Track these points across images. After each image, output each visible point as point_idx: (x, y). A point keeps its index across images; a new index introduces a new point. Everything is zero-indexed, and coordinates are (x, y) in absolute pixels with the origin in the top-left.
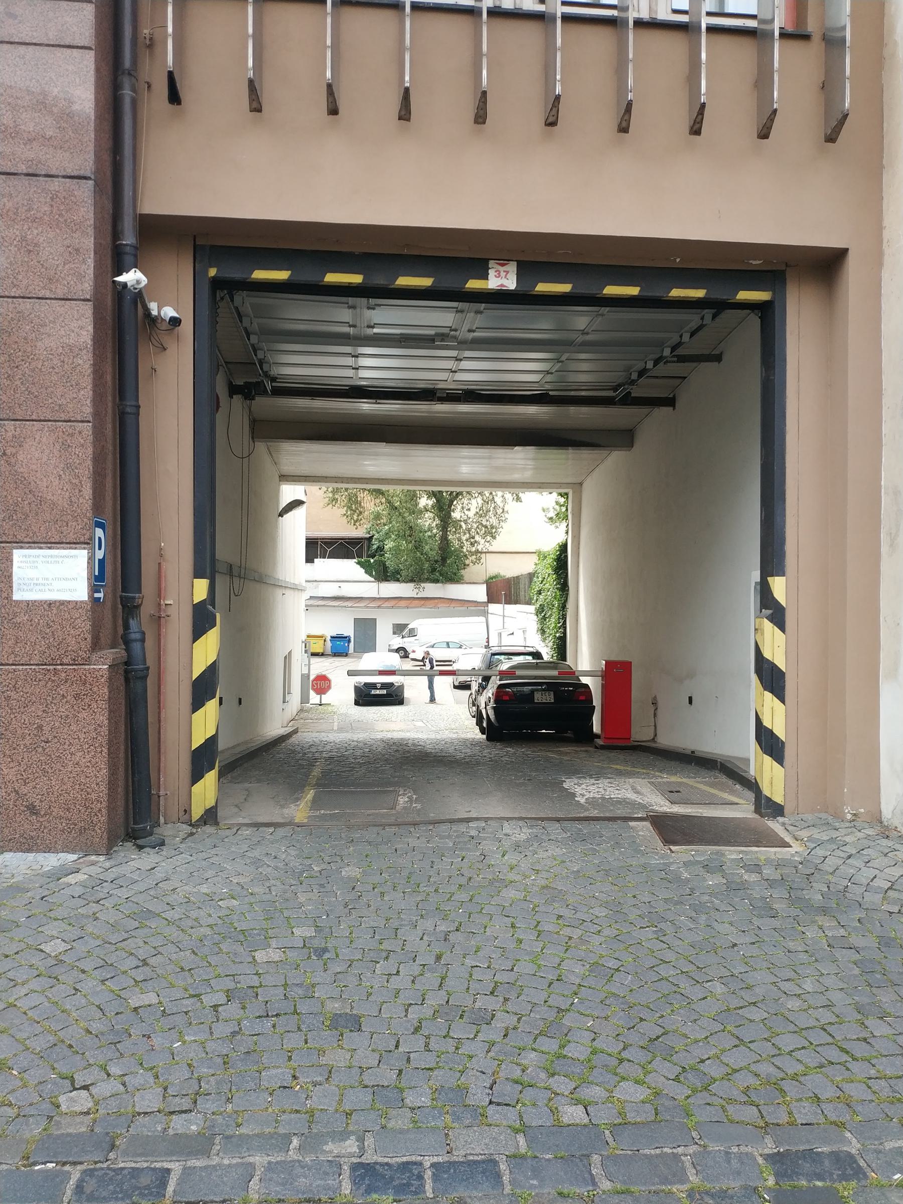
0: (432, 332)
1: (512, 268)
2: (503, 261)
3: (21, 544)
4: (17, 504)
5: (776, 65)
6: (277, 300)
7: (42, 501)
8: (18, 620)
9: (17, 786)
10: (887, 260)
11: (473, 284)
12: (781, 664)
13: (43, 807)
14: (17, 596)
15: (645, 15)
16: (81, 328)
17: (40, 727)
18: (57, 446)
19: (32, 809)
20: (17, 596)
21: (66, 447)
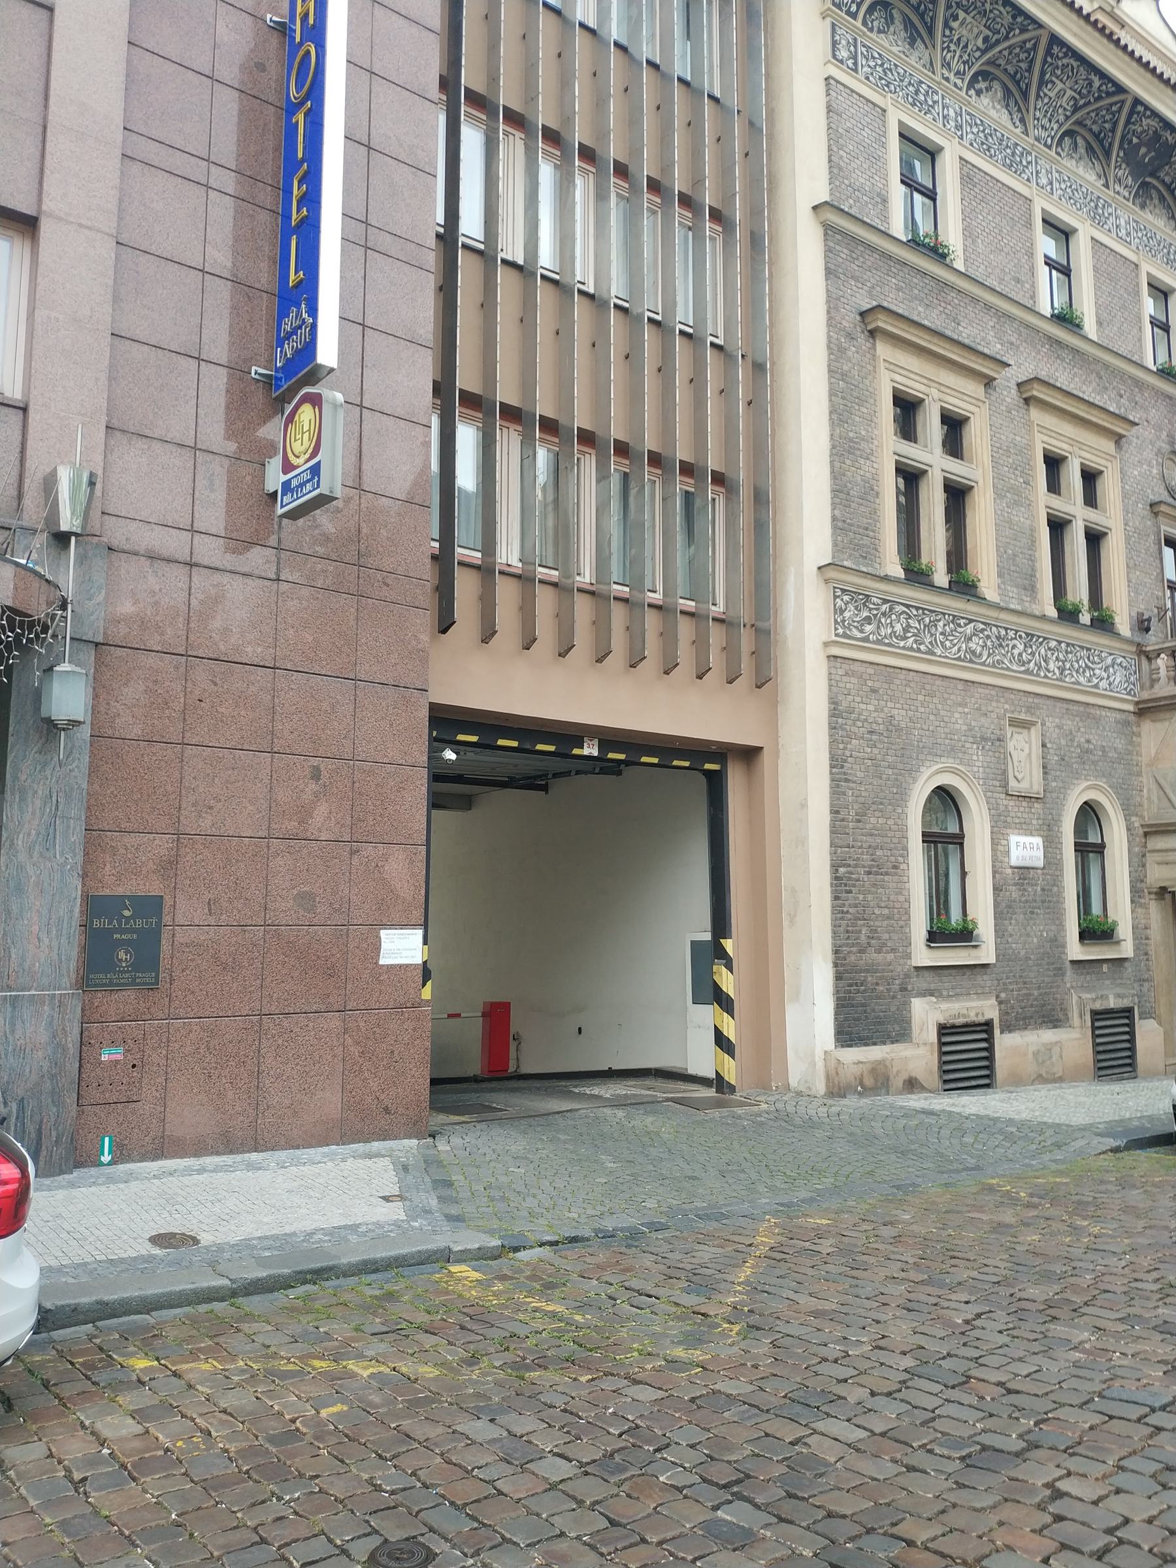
0: (540, 773)
1: (596, 742)
2: (592, 738)
3: (385, 926)
4: (383, 900)
5: (540, 109)
6: (27, 481)
7: (398, 896)
8: (382, 978)
9: (378, 1094)
10: (781, 754)
11: (576, 751)
12: (732, 1039)
13: (393, 1108)
14: (381, 962)
15: (510, 258)
16: (422, 785)
17: (392, 1052)
18: (407, 861)
19: (387, 1110)
20: (381, 962)
21: (412, 862)
